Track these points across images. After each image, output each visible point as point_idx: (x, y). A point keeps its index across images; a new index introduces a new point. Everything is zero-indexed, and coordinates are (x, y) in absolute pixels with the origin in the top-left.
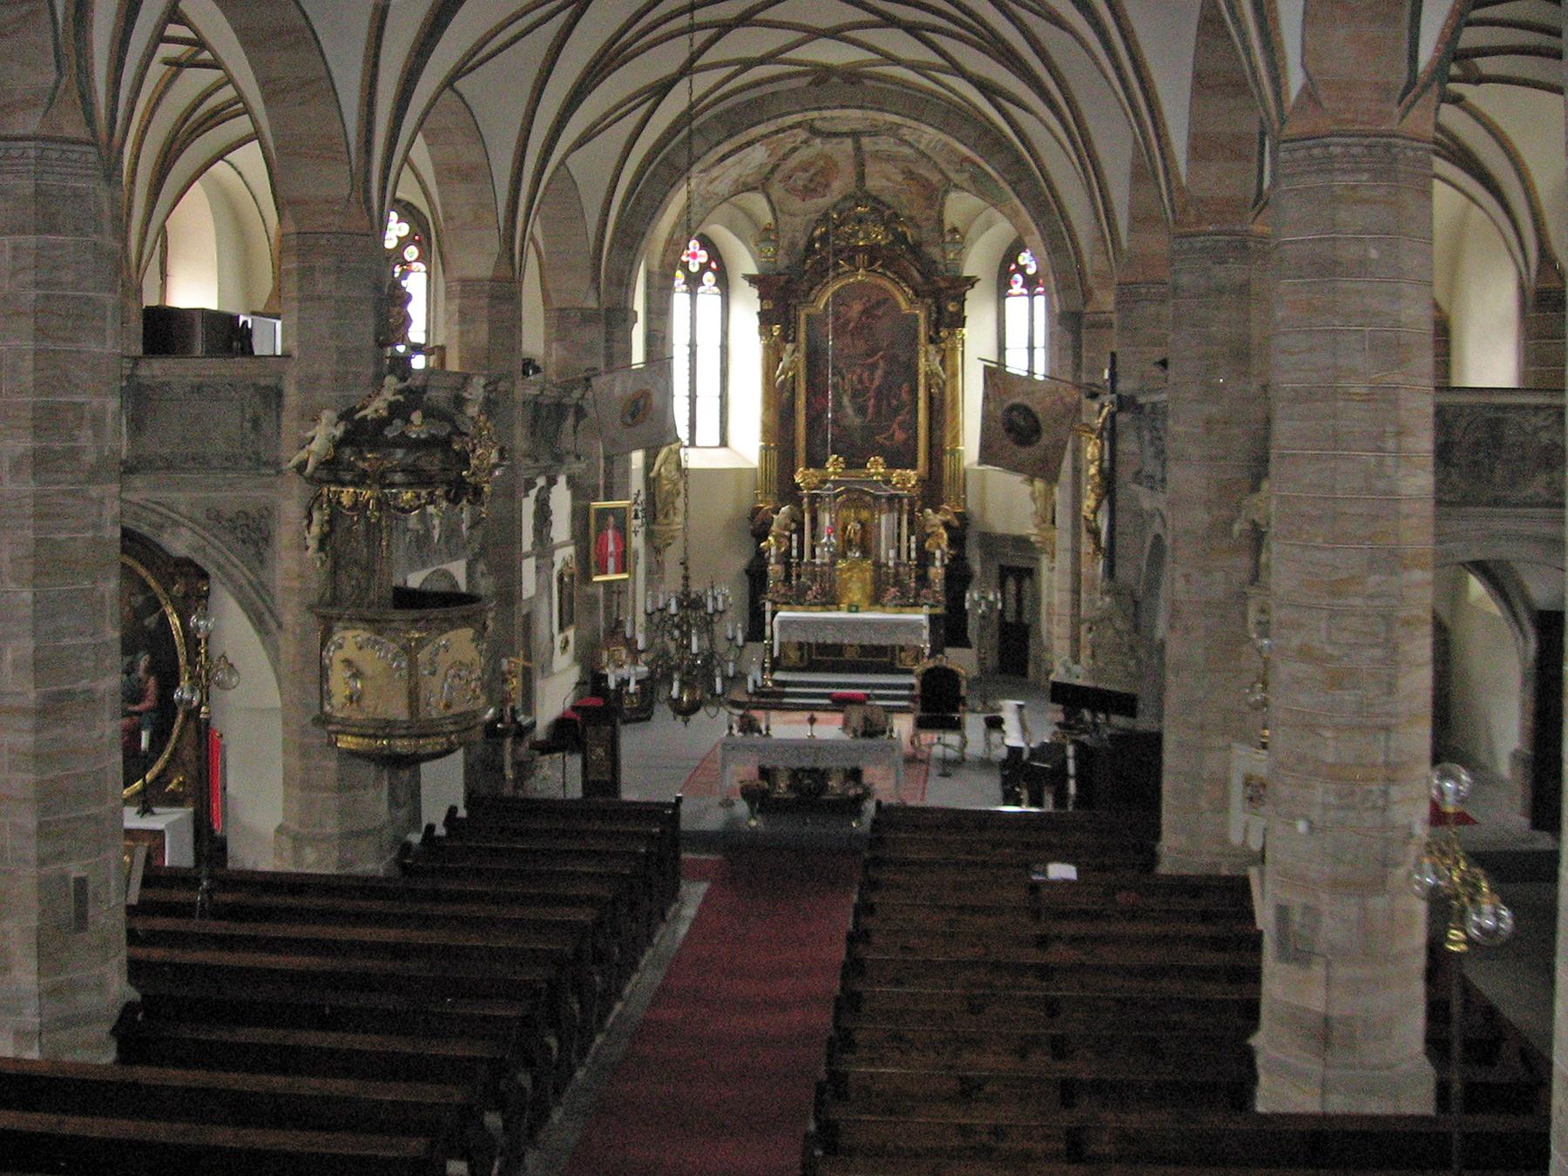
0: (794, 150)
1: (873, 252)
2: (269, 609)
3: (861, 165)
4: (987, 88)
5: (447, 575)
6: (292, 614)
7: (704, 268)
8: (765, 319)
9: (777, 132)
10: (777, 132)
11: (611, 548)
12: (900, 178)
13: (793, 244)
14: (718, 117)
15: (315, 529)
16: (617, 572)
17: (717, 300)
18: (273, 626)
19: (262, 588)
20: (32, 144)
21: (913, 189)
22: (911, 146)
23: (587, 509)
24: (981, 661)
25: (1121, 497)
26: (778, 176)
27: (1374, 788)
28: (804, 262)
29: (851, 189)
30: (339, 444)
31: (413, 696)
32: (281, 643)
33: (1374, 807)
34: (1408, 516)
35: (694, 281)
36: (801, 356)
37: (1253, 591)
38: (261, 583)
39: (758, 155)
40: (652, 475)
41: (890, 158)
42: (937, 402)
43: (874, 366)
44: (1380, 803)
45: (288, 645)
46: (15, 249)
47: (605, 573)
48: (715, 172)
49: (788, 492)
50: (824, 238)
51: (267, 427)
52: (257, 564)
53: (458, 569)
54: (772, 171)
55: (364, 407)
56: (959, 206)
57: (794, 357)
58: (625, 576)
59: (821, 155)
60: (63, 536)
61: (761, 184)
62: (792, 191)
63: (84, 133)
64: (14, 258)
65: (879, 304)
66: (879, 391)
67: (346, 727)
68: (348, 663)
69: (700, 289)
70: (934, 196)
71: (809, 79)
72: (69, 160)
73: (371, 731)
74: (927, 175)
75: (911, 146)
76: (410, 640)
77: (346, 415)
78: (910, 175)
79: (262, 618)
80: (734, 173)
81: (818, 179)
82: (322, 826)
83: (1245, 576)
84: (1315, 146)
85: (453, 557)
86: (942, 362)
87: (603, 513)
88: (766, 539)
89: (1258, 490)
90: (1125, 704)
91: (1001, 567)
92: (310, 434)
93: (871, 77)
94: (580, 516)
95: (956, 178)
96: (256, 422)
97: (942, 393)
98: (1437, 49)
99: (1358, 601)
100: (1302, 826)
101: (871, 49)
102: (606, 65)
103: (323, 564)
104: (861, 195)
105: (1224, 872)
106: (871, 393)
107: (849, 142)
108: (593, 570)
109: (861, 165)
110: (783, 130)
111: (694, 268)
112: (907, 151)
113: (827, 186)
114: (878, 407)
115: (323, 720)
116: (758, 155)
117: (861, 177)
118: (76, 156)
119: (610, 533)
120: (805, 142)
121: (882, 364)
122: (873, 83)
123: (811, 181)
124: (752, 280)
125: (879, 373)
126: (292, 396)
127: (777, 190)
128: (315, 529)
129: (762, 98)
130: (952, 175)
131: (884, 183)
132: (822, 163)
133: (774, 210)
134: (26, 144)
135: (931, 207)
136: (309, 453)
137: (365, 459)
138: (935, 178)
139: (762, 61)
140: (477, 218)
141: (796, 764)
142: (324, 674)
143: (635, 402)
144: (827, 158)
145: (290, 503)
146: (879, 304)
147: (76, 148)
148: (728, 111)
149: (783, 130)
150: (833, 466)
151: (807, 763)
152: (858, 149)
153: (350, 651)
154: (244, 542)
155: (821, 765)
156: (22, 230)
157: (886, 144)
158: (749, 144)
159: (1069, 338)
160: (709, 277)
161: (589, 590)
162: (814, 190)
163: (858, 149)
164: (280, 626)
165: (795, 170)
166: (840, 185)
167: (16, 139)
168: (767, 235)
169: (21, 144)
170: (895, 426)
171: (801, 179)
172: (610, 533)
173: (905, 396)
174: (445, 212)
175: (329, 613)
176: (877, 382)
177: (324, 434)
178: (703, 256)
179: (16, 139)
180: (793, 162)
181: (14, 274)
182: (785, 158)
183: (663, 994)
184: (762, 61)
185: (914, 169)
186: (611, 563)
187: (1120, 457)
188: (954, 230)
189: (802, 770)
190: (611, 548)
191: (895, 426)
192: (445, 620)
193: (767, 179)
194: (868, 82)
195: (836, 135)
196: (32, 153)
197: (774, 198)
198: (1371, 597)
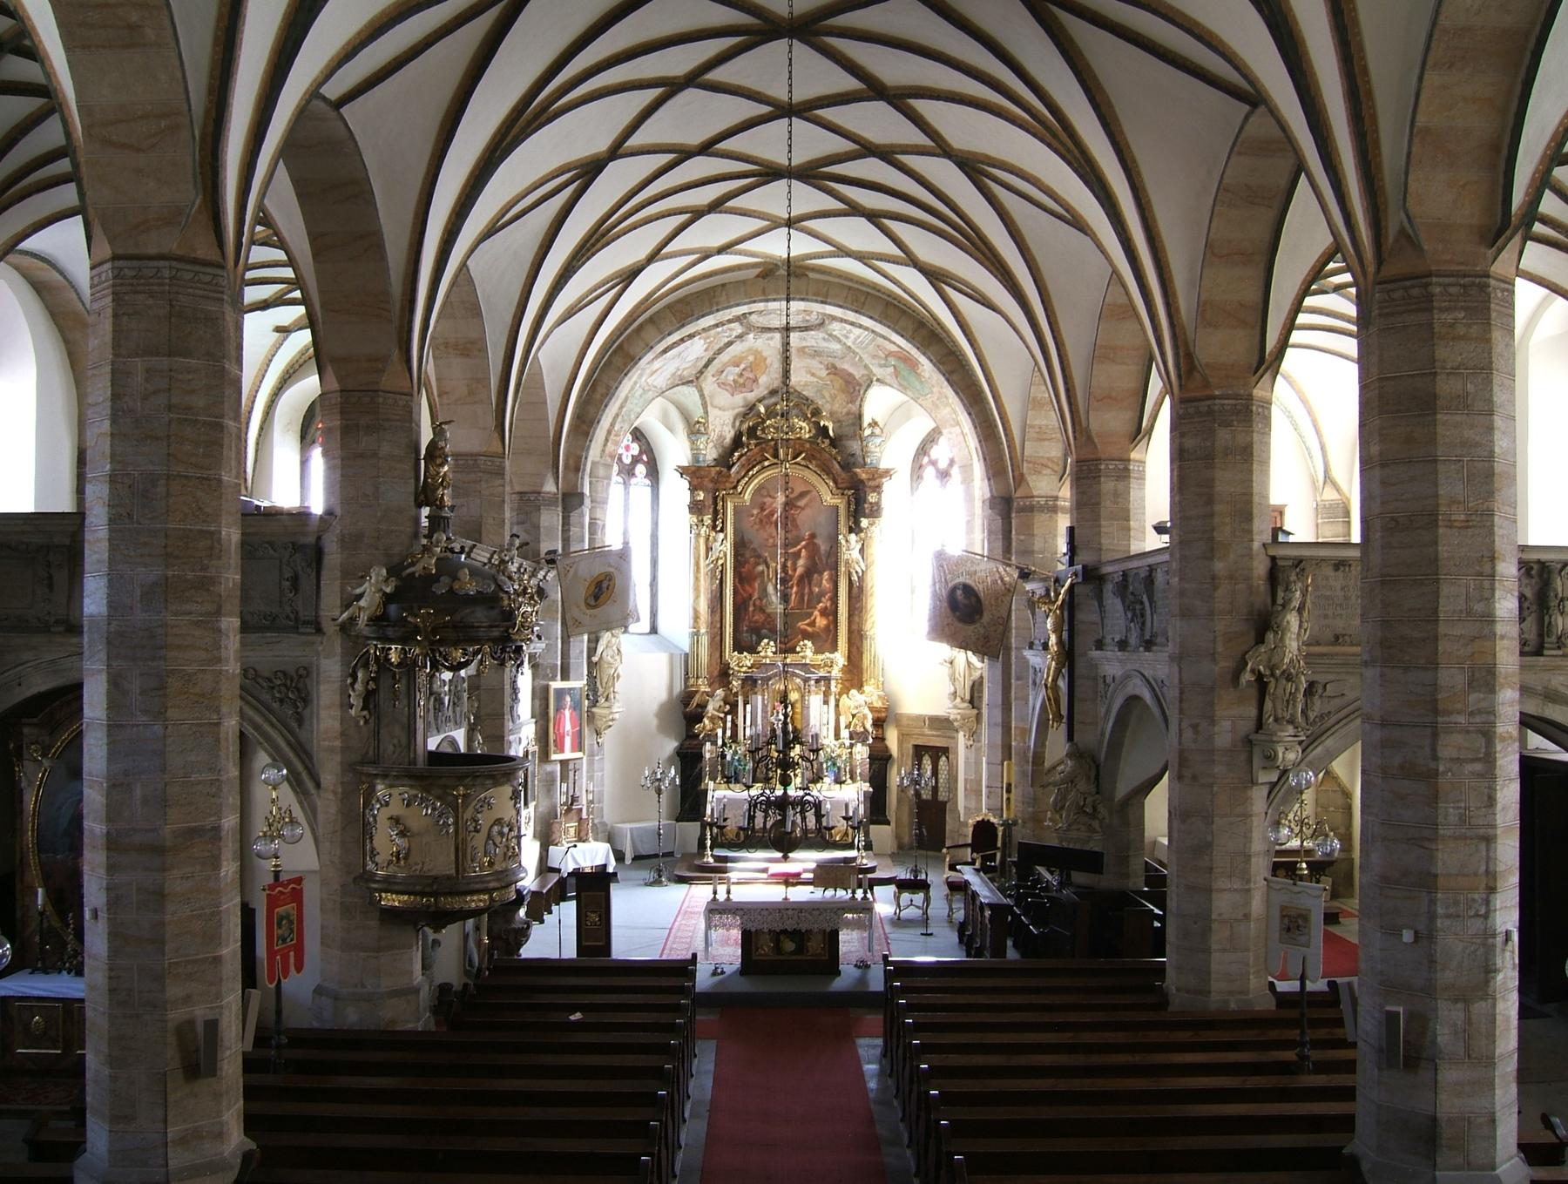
0: (730, 344)
1: (798, 448)
2: (306, 768)
3: (786, 360)
4: (935, 277)
5: (453, 742)
6: (330, 772)
7: (636, 460)
8: (696, 508)
9: (717, 326)
10: (717, 326)
11: (568, 727)
12: (824, 373)
13: (722, 437)
14: (669, 307)
15: (359, 686)
16: (573, 750)
17: (647, 492)
18: (310, 785)
19: (303, 751)
20: (167, 263)
21: (837, 385)
22: (840, 341)
23: (547, 688)
24: (898, 837)
25: (1081, 668)
26: (712, 369)
27: (1476, 896)
28: (732, 455)
29: (777, 383)
30: (388, 599)
31: (461, 852)
32: (319, 803)
33: (1477, 915)
34: (1502, 637)
35: (629, 472)
36: (728, 547)
37: (1259, 737)
38: (299, 743)
39: (696, 350)
40: (595, 659)
41: (816, 354)
42: (855, 591)
43: (797, 555)
44: (1483, 911)
45: (328, 804)
46: (148, 371)
47: (562, 751)
48: (657, 364)
49: (723, 675)
50: (752, 432)
51: (307, 584)
52: (294, 725)
53: (460, 735)
54: (706, 366)
55: (413, 564)
56: (878, 403)
57: (724, 546)
58: (579, 755)
59: (751, 351)
60: (194, 668)
61: (695, 380)
62: (722, 385)
63: (214, 255)
64: (147, 380)
65: (802, 495)
66: (801, 578)
67: (389, 885)
68: (396, 820)
69: (633, 481)
70: (854, 388)
71: (758, 271)
72: (199, 281)
73: (418, 888)
74: (851, 370)
75: (840, 341)
76: (456, 797)
77: (394, 571)
78: (834, 370)
79: (303, 779)
80: (672, 369)
81: (746, 374)
82: (363, 986)
83: (1252, 725)
84: (1413, 287)
85: (458, 725)
86: (862, 551)
87: (560, 693)
88: (701, 721)
89: (1263, 642)
90: (1092, 862)
91: (916, 747)
92: (358, 591)
93: (814, 269)
94: (541, 695)
95: (878, 372)
96: (295, 581)
97: (861, 579)
98: (1527, 194)
99: (1462, 719)
100: (1407, 936)
101: (827, 241)
102: (598, 241)
103: (366, 722)
104: (784, 389)
105: (1233, 1006)
106: (795, 581)
107: (778, 336)
108: (552, 748)
109: (786, 360)
110: (722, 324)
111: (627, 460)
112: (835, 346)
113: (755, 381)
114: (801, 595)
115: (367, 877)
116: (696, 350)
117: (786, 374)
118: (208, 279)
119: (567, 713)
120: (740, 337)
121: (804, 553)
122: (817, 276)
123: (741, 375)
124: (683, 471)
125: (801, 562)
126: (333, 555)
127: (709, 384)
128: (359, 686)
129: (714, 288)
130: (875, 370)
131: (810, 379)
132: (751, 358)
133: (705, 405)
134: (162, 263)
135: (852, 402)
136: (360, 609)
137: (416, 616)
138: (858, 373)
139: (722, 250)
140: (471, 393)
141: (778, 927)
142: (366, 831)
143: (599, 585)
144: (756, 353)
145: (331, 667)
146: (802, 495)
147: (209, 270)
148: (680, 301)
149: (722, 324)
150: (768, 649)
151: (789, 925)
152: (786, 345)
153: (396, 808)
154: (281, 701)
155: (803, 927)
156: (156, 352)
157: (814, 339)
158: (691, 336)
159: (999, 522)
160: (641, 469)
161: (549, 768)
162: (744, 385)
163: (786, 345)
164: (318, 785)
165: (726, 365)
166: (769, 378)
167: (150, 258)
168: (695, 429)
169: (155, 263)
170: (816, 613)
171: (732, 374)
172: (567, 713)
173: (826, 584)
174: (439, 387)
175: (365, 768)
176: (800, 570)
177: (372, 589)
178: (635, 449)
179: (150, 258)
180: (724, 357)
181: (145, 398)
182: (720, 351)
183: (712, 1137)
184: (722, 250)
185: (839, 365)
186: (568, 741)
187: (1079, 627)
188: (874, 424)
189: (784, 932)
190: (568, 727)
191: (816, 613)
192: (491, 777)
193: (701, 372)
194: (811, 275)
195: (769, 330)
196: (166, 273)
197: (706, 393)
198: (1471, 714)
